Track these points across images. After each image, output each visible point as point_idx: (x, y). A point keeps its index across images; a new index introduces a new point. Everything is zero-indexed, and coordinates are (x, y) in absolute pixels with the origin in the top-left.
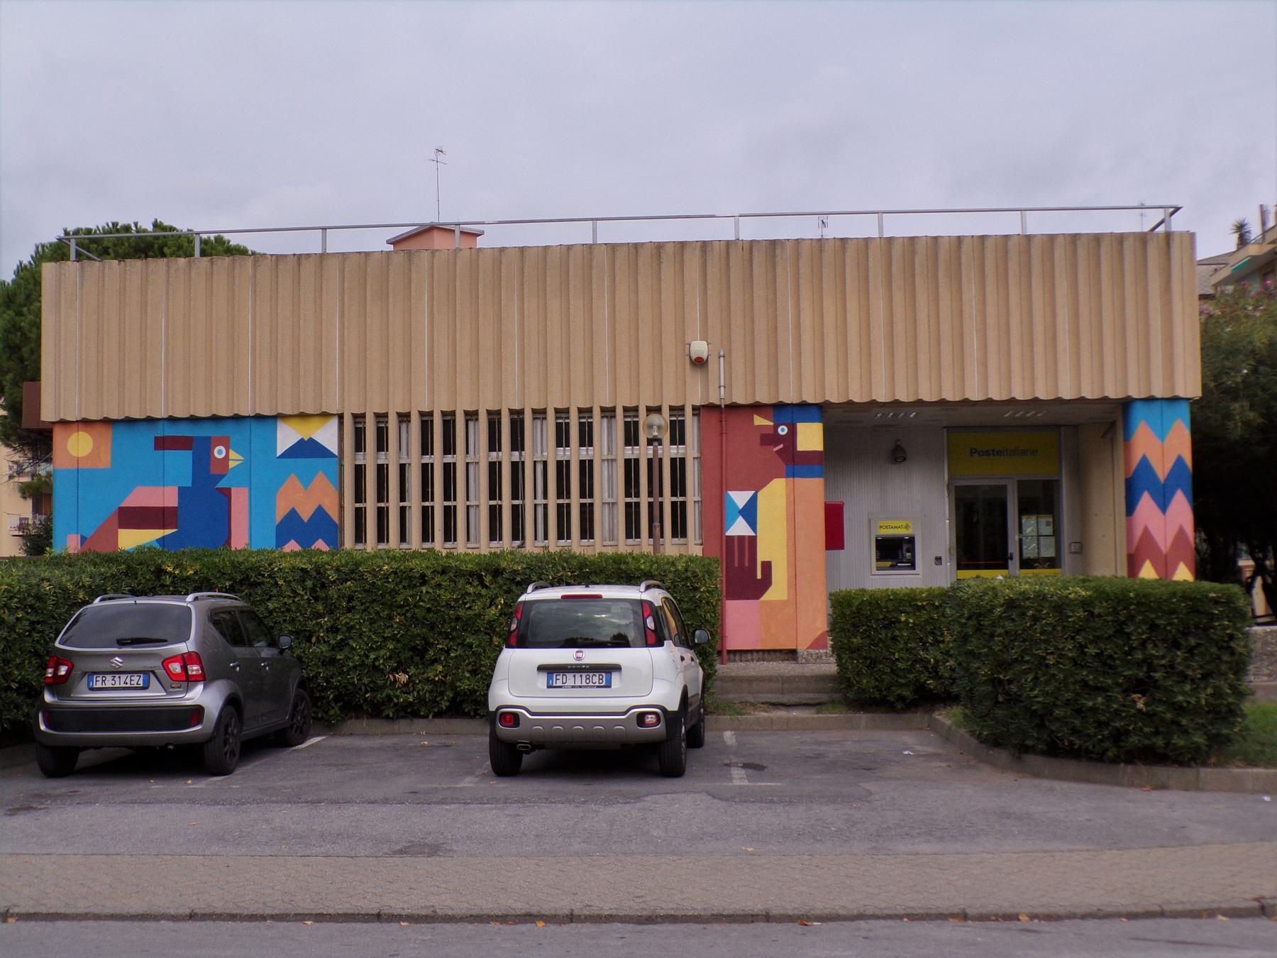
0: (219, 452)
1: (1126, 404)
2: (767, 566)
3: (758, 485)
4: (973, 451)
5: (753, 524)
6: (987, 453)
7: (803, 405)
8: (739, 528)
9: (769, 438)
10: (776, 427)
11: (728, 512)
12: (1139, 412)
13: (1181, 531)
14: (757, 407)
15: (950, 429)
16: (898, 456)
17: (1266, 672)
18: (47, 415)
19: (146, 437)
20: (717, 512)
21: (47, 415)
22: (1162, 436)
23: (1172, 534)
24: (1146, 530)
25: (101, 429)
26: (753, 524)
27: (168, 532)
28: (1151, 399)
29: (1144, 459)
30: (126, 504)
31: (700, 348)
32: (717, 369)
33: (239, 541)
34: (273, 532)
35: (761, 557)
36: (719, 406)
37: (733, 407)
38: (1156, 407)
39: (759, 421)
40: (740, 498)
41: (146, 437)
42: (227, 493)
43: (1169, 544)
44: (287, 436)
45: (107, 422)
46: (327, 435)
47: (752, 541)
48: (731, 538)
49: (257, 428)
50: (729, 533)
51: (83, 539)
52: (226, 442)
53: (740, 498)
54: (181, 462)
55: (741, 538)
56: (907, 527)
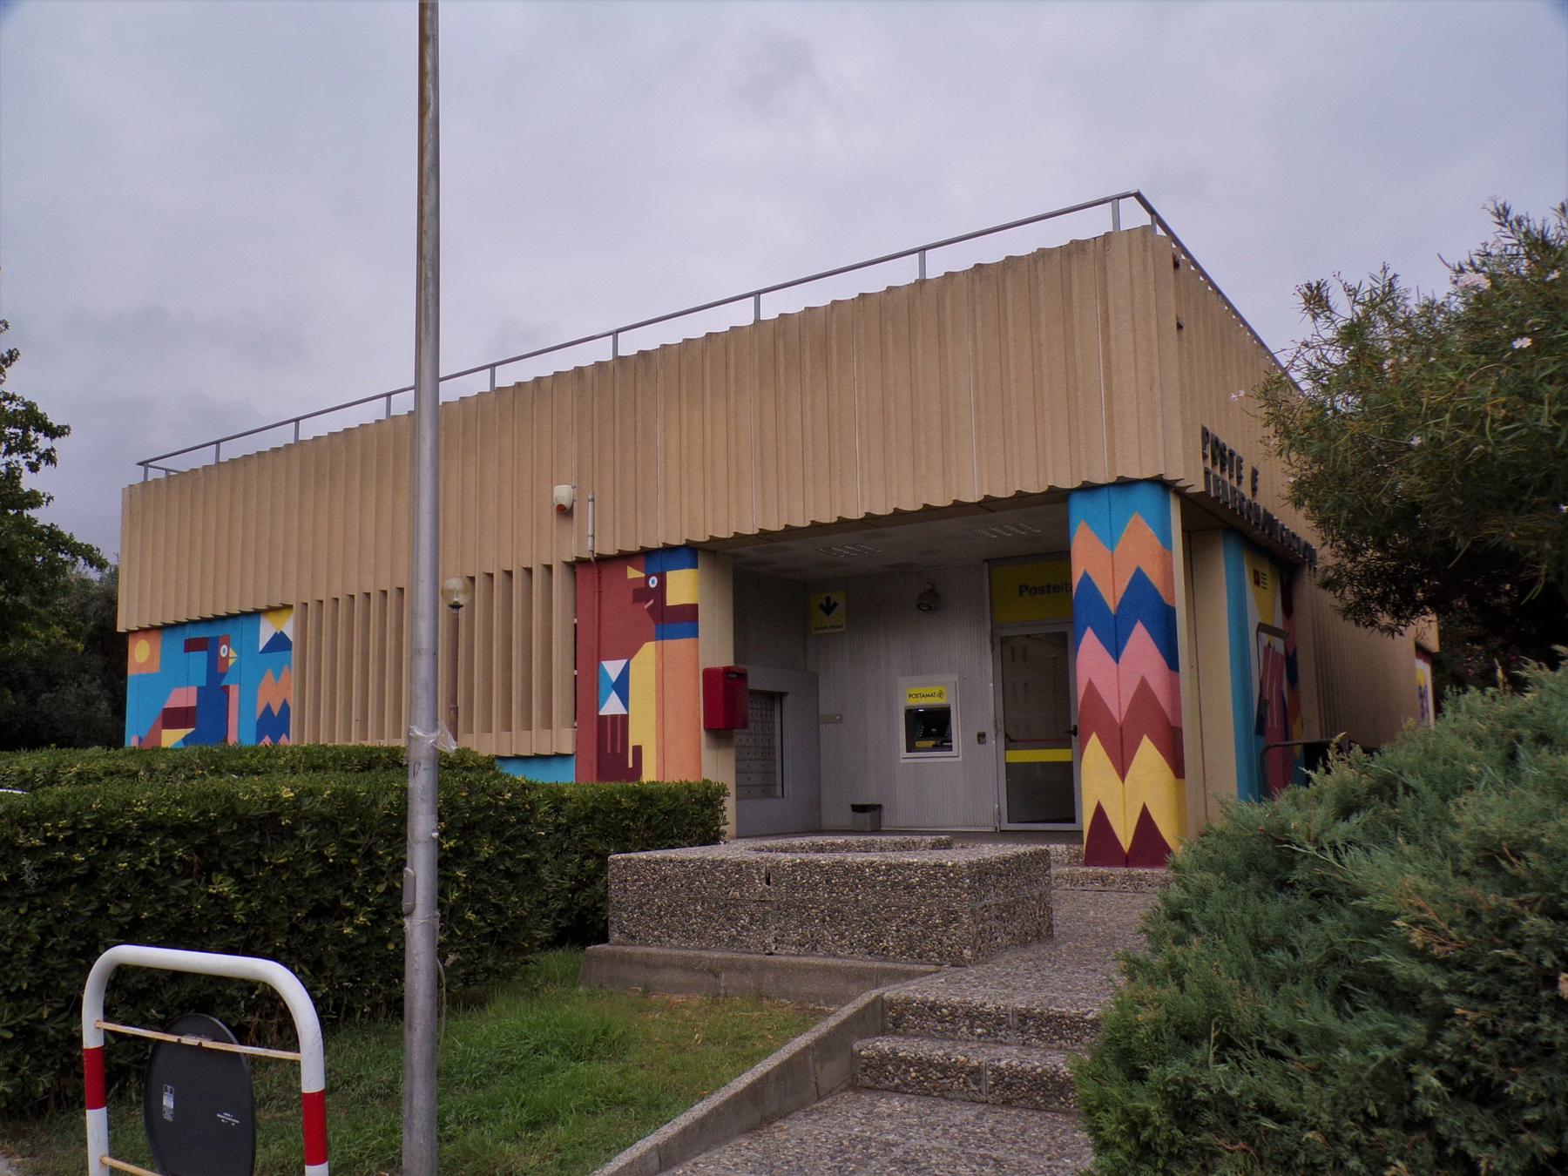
0: (224, 651)
1: (1058, 498)
2: (638, 750)
3: (629, 653)
4: (1023, 589)
5: (625, 700)
6: (1041, 590)
7: (668, 549)
8: (612, 706)
9: (642, 593)
10: (647, 579)
11: (603, 687)
12: (1078, 506)
13: (1144, 685)
14: (625, 558)
15: (991, 562)
16: (931, 602)
17: (795, 937)
18: (121, 628)
19: (178, 640)
20: (586, 690)
21: (121, 628)
22: (1112, 543)
23: (1129, 691)
24: (1090, 686)
25: (154, 635)
26: (625, 700)
27: (190, 730)
28: (1088, 488)
29: (1086, 578)
30: (170, 704)
31: (563, 493)
32: (586, 515)
33: (232, 739)
34: (254, 725)
35: (633, 741)
36: (588, 561)
37: (602, 560)
38: (1102, 499)
39: (633, 573)
40: (613, 668)
41: (178, 640)
42: (226, 689)
43: (1125, 708)
44: (267, 630)
45: (153, 629)
46: (288, 626)
47: (625, 718)
48: (602, 719)
49: (245, 624)
50: (601, 713)
51: (140, 740)
52: (227, 641)
53: (613, 668)
54: (199, 659)
55: (614, 717)
56: (940, 695)
